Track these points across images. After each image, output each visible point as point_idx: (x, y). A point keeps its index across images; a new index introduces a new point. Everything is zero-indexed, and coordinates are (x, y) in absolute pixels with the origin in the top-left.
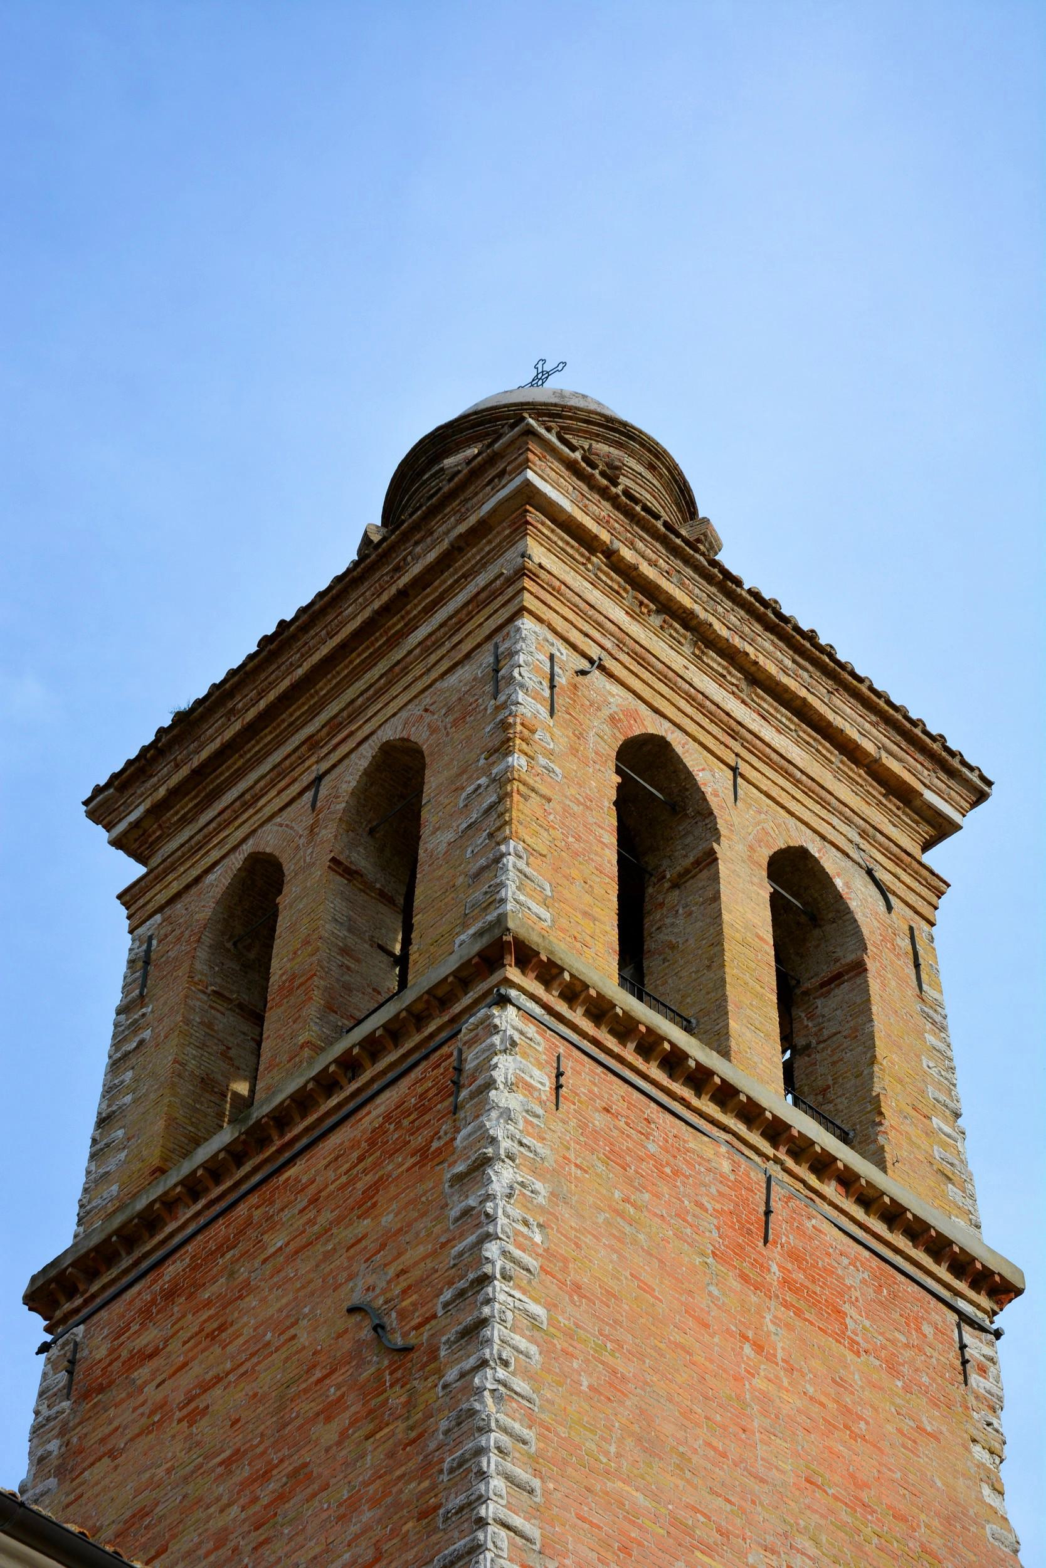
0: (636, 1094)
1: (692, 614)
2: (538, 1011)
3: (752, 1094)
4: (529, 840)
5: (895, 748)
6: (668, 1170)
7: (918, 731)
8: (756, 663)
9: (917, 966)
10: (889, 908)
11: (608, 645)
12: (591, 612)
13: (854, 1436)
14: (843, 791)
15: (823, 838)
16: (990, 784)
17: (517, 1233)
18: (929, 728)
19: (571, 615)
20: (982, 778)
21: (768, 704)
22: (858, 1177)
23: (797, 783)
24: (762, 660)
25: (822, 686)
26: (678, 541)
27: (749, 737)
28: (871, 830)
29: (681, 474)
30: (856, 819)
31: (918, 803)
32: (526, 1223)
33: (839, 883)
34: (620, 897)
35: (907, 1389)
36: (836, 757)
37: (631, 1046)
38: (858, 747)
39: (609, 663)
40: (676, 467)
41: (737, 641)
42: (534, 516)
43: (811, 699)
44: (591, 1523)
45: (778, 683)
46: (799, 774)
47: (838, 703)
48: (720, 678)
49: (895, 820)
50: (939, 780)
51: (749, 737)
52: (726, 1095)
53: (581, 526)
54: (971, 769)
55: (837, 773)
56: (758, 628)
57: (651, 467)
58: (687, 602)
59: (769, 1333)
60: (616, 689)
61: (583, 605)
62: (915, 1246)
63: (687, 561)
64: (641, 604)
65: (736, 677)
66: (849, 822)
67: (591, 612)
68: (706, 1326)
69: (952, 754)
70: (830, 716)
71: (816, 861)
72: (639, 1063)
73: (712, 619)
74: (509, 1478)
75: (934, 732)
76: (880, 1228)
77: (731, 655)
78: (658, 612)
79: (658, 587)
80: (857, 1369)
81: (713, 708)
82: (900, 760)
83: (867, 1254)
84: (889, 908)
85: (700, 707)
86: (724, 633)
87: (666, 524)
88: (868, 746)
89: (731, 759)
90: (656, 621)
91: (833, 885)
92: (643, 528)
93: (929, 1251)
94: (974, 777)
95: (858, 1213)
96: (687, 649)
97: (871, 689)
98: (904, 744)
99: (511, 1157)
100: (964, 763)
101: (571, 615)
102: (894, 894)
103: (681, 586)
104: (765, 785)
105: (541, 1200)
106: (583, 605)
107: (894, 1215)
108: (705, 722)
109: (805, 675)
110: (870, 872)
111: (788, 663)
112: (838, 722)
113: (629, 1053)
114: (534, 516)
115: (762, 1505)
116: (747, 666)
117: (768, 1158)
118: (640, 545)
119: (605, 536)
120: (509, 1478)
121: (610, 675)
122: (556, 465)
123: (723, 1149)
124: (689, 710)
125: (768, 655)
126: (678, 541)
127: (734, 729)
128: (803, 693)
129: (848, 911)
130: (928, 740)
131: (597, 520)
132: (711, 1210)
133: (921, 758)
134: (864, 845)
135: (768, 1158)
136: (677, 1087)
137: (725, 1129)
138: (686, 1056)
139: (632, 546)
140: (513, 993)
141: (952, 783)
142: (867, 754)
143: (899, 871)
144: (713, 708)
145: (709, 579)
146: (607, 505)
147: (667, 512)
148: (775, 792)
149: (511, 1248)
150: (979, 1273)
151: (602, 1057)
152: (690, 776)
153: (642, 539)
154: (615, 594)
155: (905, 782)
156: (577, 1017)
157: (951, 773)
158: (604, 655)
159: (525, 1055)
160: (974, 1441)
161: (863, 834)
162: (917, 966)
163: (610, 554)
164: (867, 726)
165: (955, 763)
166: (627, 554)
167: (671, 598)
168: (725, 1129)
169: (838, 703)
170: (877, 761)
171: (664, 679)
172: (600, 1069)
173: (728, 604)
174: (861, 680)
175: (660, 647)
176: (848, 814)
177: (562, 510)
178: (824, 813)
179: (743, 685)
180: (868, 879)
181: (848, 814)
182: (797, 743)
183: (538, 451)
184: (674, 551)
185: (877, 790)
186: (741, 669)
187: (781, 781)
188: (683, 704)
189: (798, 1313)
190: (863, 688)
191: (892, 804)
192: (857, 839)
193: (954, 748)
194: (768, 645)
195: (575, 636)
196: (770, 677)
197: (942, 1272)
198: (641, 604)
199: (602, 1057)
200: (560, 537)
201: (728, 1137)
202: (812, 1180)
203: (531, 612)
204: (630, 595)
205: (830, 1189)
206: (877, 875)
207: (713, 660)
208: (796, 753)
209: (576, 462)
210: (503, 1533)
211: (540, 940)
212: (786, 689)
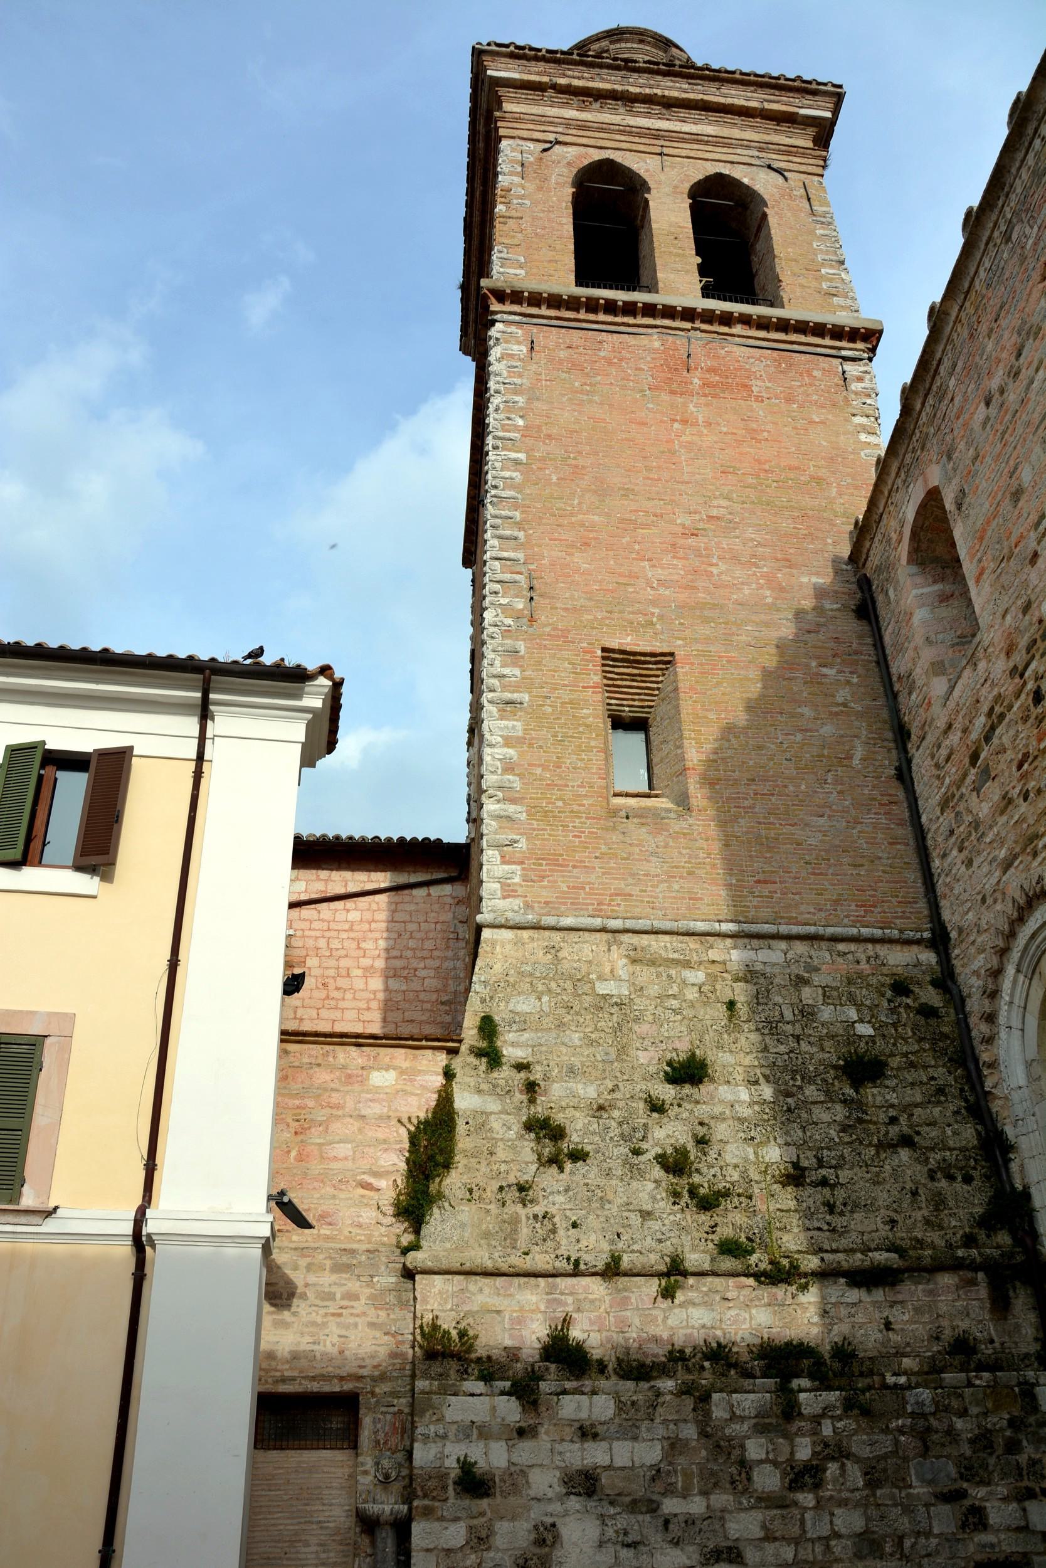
0: (590, 333)
1: (614, 91)
2: (517, 318)
3: (665, 302)
4: (506, 241)
5: (772, 97)
6: (615, 360)
7: (782, 81)
8: (664, 96)
9: (809, 199)
10: (786, 179)
11: (560, 130)
12: (543, 119)
13: (759, 441)
14: (736, 133)
15: (732, 163)
16: (840, 87)
17: (503, 426)
18: (788, 76)
19: (531, 127)
20: (834, 86)
21: (683, 113)
22: (751, 316)
23: (707, 143)
24: (666, 93)
25: (712, 88)
26: (590, 59)
27: (667, 134)
28: (764, 146)
29: (661, 36)
30: (752, 144)
31: (799, 119)
32: (509, 419)
33: (746, 181)
34: (575, 244)
35: (801, 406)
36: (737, 120)
37: (583, 311)
38: (748, 108)
39: (561, 138)
40: (656, 34)
41: (647, 91)
42: (502, 91)
43: (706, 98)
44: (561, 540)
45: (683, 100)
46: (706, 138)
47: (726, 91)
48: (647, 115)
49: (790, 134)
50: (808, 100)
51: (667, 134)
52: (669, 312)
53: (529, 82)
54: (825, 84)
55: (742, 128)
56: (659, 78)
57: (641, 41)
58: (607, 86)
59: (692, 413)
60: (570, 149)
61: (537, 118)
62: (616, 316)
63: (601, 66)
64: (584, 101)
65: (657, 109)
66: (748, 147)
67: (543, 119)
68: (645, 424)
69: (810, 82)
70: (722, 100)
71: (728, 176)
72: (592, 317)
73: (627, 88)
74: (499, 537)
75: (793, 77)
76: (781, 336)
77: (649, 100)
78: (596, 100)
79: (588, 88)
80: (759, 410)
81: (638, 130)
82: (778, 102)
83: (769, 352)
84: (786, 179)
85: (630, 134)
86: (638, 90)
87: (645, 62)
88: (754, 104)
89: (658, 150)
90: (597, 105)
91: (742, 183)
92: (568, 64)
93: (814, 334)
94: (829, 88)
95: (762, 334)
96: (622, 110)
97: (742, 74)
98: (777, 93)
99: (497, 392)
100: (819, 84)
101: (531, 127)
102: (785, 170)
103: (603, 80)
104: (684, 153)
105: (520, 404)
106: (537, 118)
107: (802, 327)
108: (637, 140)
109: (699, 87)
110: (769, 167)
111: (686, 86)
112: (729, 101)
113: (582, 315)
114: (502, 91)
115: (687, 494)
116: (662, 100)
117: (689, 330)
118: (569, 73)
119: (545, 79)
120: (499, 537)
121: (566, 144)
122: (503, 60)
123: (655, 337)
124: (623, 138)
125: (671, 88)
126: (590, 59)
127: (656, 134)
128: (700, 97)
129: (754, 192)
130: (790, 83)
131: (539, 74)
132: (646, 368)
133: (791, 95)
134: (761, 155)
135: (689, 330)
136: (618, 319)
137: (656, 327)
138: (616, 301)
139: (565, 76)
140: (498, 317)
141: (817, 98)
142: (755, 109)
143: (791, 158)
144: (638, 130)
145: (618, 68)
146: (542, 63)
147: (660, 55)
148: (692, 154)
149: (501, 434)
150: (849, 332)
151: (565, 324)
152: (629, 169)
153: (569, 69)
154: (566, 105)
155: (784, 112)
156: (544, 311)
157: (814, 93)
158: (558, 136)
159: (507, 342)
160: (854, 415)
161: (760, 149)
162: (809, 199)
163: (554, 87)
164: (749, 94)
165: (814, 86)
166: (562, 81)
167: (598, 90)
168: (656, 327)
169: (726, 91)
170: (763, 110)
171: (600, 130)
172: (563, 330)
173: (636, 75)
174: (733, 72)
175: (606, 117)
176: (747, 144)
177: (515, 80)
178: (730, 150)
179: (664, 111)
180: (769, 171)
181: (747, 144)
182: (710, 124)
183: (489, 58)
184: (591, 65)
185: (771, 125)
186: (658, 104)
187: (696, 147)
188: (618, 137)
189: (714, 396)
190: (737, 76)
191: (784, 127)
192: (757, 154)
193: (809, 79)
194: (670, 84)
195: (537, 135)
196: (677, 99)
197: (828, 341)
198: (584, 101)
199: (565, 324)
200: (522, 93)
201: (659, 330)
202: (725, 329)
203: (505, 137)
204: (575, 100)
205: (738, 329)
206: (775, 166)
207: (640, 107)
208: (710, 130)
209: (512, 52)
210: (497, 563)
211: (504, 284)
212: (689, 100)
